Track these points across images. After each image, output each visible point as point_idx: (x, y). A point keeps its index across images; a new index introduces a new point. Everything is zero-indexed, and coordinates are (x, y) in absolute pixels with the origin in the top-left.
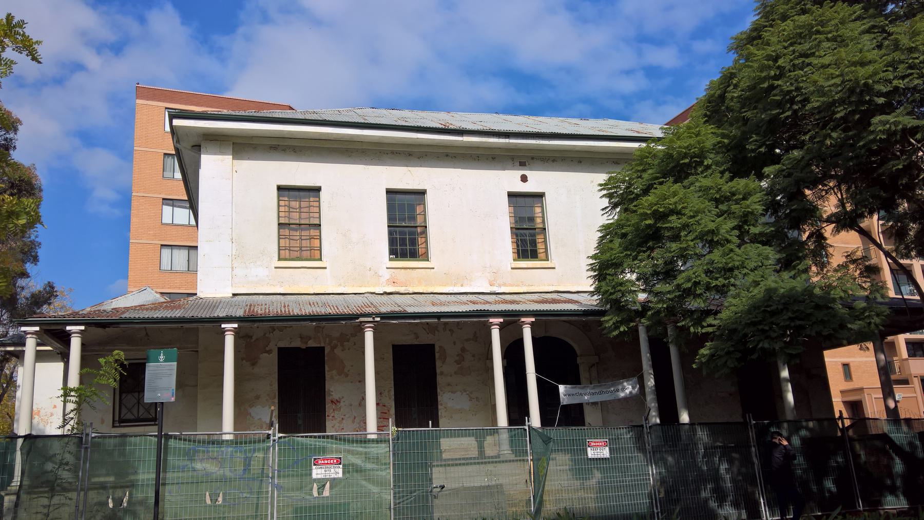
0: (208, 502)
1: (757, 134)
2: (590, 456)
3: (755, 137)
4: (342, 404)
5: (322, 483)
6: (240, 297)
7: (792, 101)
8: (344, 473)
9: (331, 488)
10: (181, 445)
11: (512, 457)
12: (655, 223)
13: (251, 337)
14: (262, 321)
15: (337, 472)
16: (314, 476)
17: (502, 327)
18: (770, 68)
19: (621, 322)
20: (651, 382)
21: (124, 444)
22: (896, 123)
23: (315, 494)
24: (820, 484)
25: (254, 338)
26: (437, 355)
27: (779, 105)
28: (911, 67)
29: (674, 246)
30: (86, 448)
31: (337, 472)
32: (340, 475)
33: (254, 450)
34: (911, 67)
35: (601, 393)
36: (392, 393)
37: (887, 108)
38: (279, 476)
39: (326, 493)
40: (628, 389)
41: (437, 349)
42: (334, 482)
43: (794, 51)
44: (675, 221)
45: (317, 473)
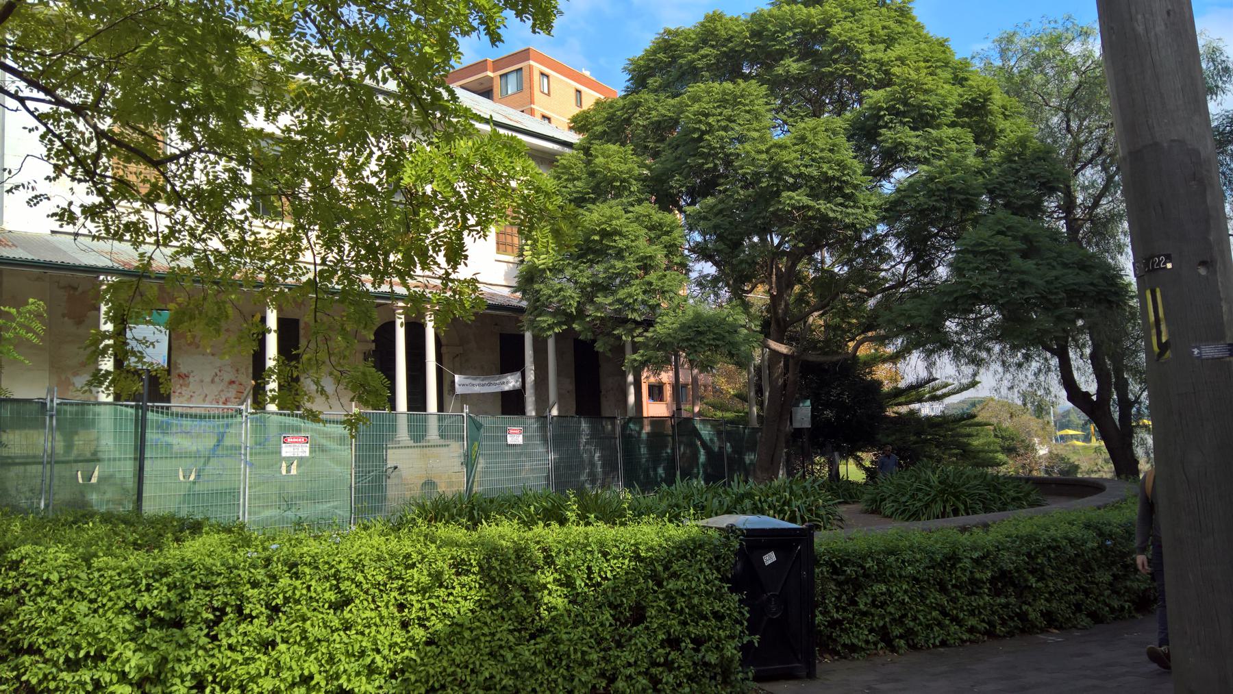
0: (181, 478)
1: (680, 174)
2: (509, 442)
3: (677, 177)
4: (191, 379)
5: (290, 462)
6: (63, 236)
7: (715, 156)
8: (311, 452)
9: (299, 466)
10: (160, 418)
11: (411, 443)
12: (601, 240)
13: (75, 289)
14: (52, 268)
15: (304, 450)
16: (284, 454)
17: (406, 312)
18: (700, 122)
19: (559, 324)
20: (531, 377)
21: (83, 413)
22: (798, 201)
23: (284, 472)
24: (655, 470)
25: (80, 290)
26: (302, 332)
27: (705, 156)
28: (813, 160)
29: (619, 265)
30: (51, 417)
31: (304, 450)
32: (307, 454)
33: (227, 426)
34: (813, 160)
35: (490, 384)
36: (251, 370)
37: (794, 187)
38: (251, 454)
39: (294, 471)
40: (511, 382)
41: (302, 325)
42: (301, 460)
43: (720, 114)
44: (622, 243)
45: (287, 451)
